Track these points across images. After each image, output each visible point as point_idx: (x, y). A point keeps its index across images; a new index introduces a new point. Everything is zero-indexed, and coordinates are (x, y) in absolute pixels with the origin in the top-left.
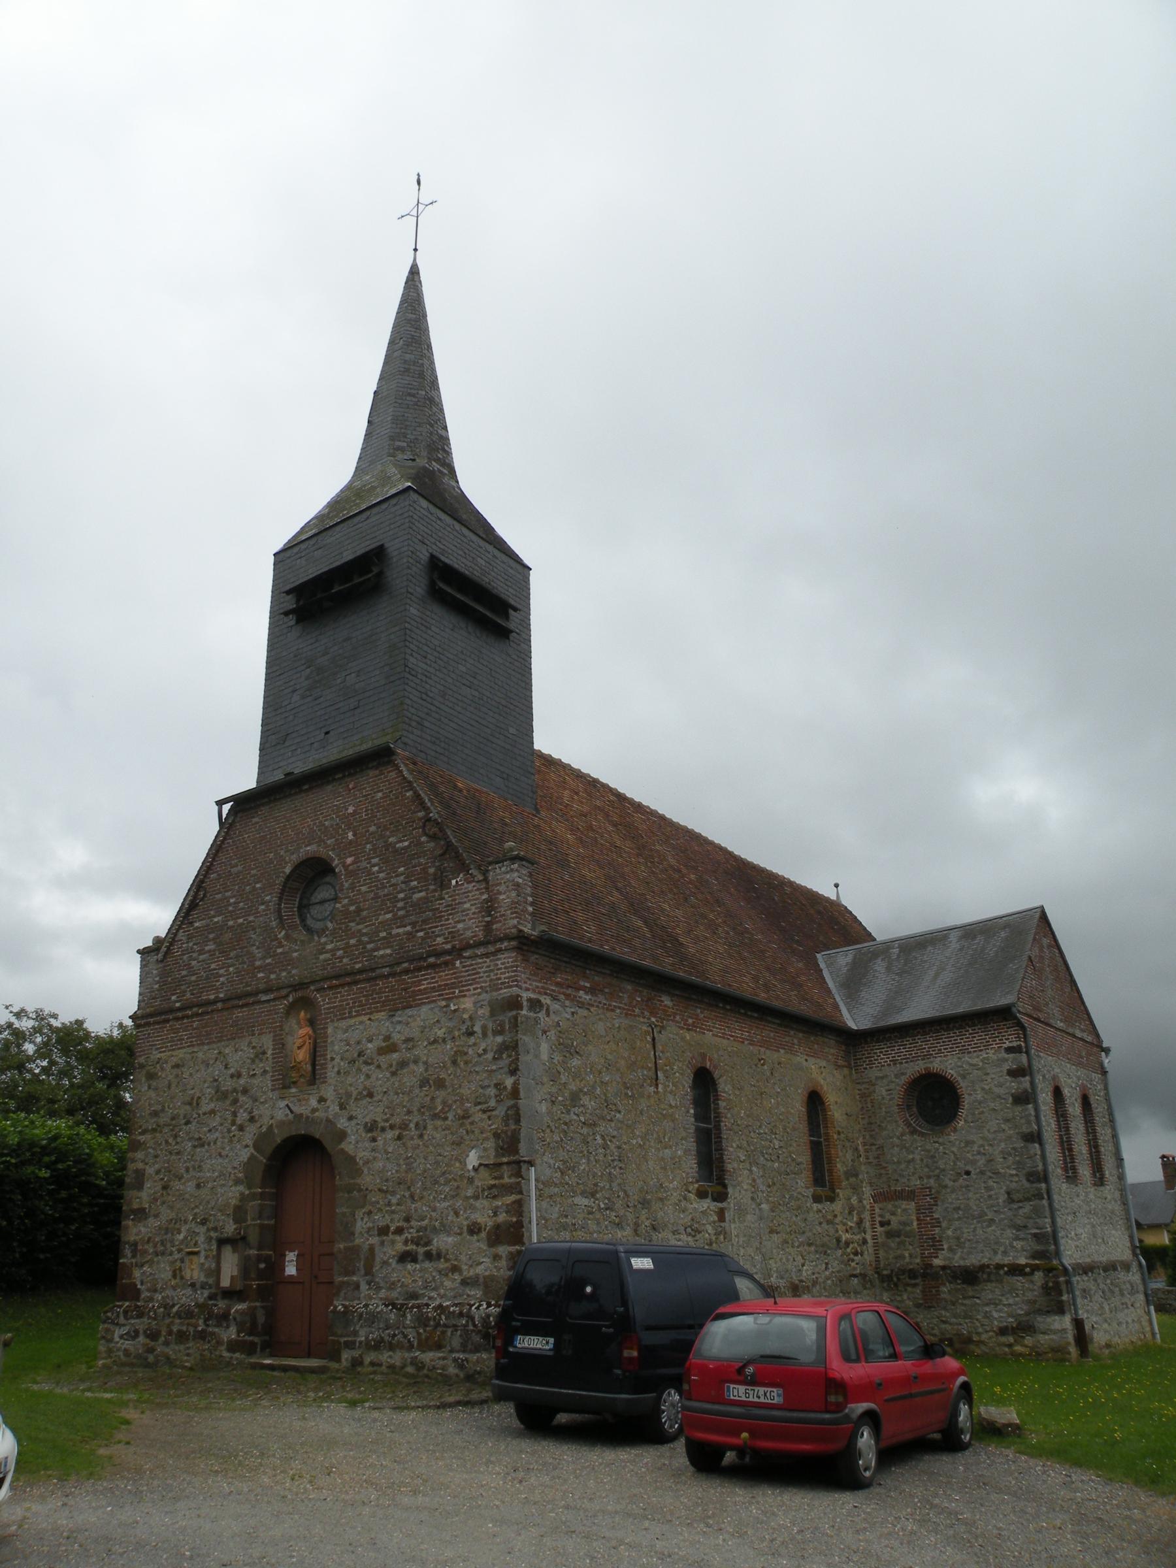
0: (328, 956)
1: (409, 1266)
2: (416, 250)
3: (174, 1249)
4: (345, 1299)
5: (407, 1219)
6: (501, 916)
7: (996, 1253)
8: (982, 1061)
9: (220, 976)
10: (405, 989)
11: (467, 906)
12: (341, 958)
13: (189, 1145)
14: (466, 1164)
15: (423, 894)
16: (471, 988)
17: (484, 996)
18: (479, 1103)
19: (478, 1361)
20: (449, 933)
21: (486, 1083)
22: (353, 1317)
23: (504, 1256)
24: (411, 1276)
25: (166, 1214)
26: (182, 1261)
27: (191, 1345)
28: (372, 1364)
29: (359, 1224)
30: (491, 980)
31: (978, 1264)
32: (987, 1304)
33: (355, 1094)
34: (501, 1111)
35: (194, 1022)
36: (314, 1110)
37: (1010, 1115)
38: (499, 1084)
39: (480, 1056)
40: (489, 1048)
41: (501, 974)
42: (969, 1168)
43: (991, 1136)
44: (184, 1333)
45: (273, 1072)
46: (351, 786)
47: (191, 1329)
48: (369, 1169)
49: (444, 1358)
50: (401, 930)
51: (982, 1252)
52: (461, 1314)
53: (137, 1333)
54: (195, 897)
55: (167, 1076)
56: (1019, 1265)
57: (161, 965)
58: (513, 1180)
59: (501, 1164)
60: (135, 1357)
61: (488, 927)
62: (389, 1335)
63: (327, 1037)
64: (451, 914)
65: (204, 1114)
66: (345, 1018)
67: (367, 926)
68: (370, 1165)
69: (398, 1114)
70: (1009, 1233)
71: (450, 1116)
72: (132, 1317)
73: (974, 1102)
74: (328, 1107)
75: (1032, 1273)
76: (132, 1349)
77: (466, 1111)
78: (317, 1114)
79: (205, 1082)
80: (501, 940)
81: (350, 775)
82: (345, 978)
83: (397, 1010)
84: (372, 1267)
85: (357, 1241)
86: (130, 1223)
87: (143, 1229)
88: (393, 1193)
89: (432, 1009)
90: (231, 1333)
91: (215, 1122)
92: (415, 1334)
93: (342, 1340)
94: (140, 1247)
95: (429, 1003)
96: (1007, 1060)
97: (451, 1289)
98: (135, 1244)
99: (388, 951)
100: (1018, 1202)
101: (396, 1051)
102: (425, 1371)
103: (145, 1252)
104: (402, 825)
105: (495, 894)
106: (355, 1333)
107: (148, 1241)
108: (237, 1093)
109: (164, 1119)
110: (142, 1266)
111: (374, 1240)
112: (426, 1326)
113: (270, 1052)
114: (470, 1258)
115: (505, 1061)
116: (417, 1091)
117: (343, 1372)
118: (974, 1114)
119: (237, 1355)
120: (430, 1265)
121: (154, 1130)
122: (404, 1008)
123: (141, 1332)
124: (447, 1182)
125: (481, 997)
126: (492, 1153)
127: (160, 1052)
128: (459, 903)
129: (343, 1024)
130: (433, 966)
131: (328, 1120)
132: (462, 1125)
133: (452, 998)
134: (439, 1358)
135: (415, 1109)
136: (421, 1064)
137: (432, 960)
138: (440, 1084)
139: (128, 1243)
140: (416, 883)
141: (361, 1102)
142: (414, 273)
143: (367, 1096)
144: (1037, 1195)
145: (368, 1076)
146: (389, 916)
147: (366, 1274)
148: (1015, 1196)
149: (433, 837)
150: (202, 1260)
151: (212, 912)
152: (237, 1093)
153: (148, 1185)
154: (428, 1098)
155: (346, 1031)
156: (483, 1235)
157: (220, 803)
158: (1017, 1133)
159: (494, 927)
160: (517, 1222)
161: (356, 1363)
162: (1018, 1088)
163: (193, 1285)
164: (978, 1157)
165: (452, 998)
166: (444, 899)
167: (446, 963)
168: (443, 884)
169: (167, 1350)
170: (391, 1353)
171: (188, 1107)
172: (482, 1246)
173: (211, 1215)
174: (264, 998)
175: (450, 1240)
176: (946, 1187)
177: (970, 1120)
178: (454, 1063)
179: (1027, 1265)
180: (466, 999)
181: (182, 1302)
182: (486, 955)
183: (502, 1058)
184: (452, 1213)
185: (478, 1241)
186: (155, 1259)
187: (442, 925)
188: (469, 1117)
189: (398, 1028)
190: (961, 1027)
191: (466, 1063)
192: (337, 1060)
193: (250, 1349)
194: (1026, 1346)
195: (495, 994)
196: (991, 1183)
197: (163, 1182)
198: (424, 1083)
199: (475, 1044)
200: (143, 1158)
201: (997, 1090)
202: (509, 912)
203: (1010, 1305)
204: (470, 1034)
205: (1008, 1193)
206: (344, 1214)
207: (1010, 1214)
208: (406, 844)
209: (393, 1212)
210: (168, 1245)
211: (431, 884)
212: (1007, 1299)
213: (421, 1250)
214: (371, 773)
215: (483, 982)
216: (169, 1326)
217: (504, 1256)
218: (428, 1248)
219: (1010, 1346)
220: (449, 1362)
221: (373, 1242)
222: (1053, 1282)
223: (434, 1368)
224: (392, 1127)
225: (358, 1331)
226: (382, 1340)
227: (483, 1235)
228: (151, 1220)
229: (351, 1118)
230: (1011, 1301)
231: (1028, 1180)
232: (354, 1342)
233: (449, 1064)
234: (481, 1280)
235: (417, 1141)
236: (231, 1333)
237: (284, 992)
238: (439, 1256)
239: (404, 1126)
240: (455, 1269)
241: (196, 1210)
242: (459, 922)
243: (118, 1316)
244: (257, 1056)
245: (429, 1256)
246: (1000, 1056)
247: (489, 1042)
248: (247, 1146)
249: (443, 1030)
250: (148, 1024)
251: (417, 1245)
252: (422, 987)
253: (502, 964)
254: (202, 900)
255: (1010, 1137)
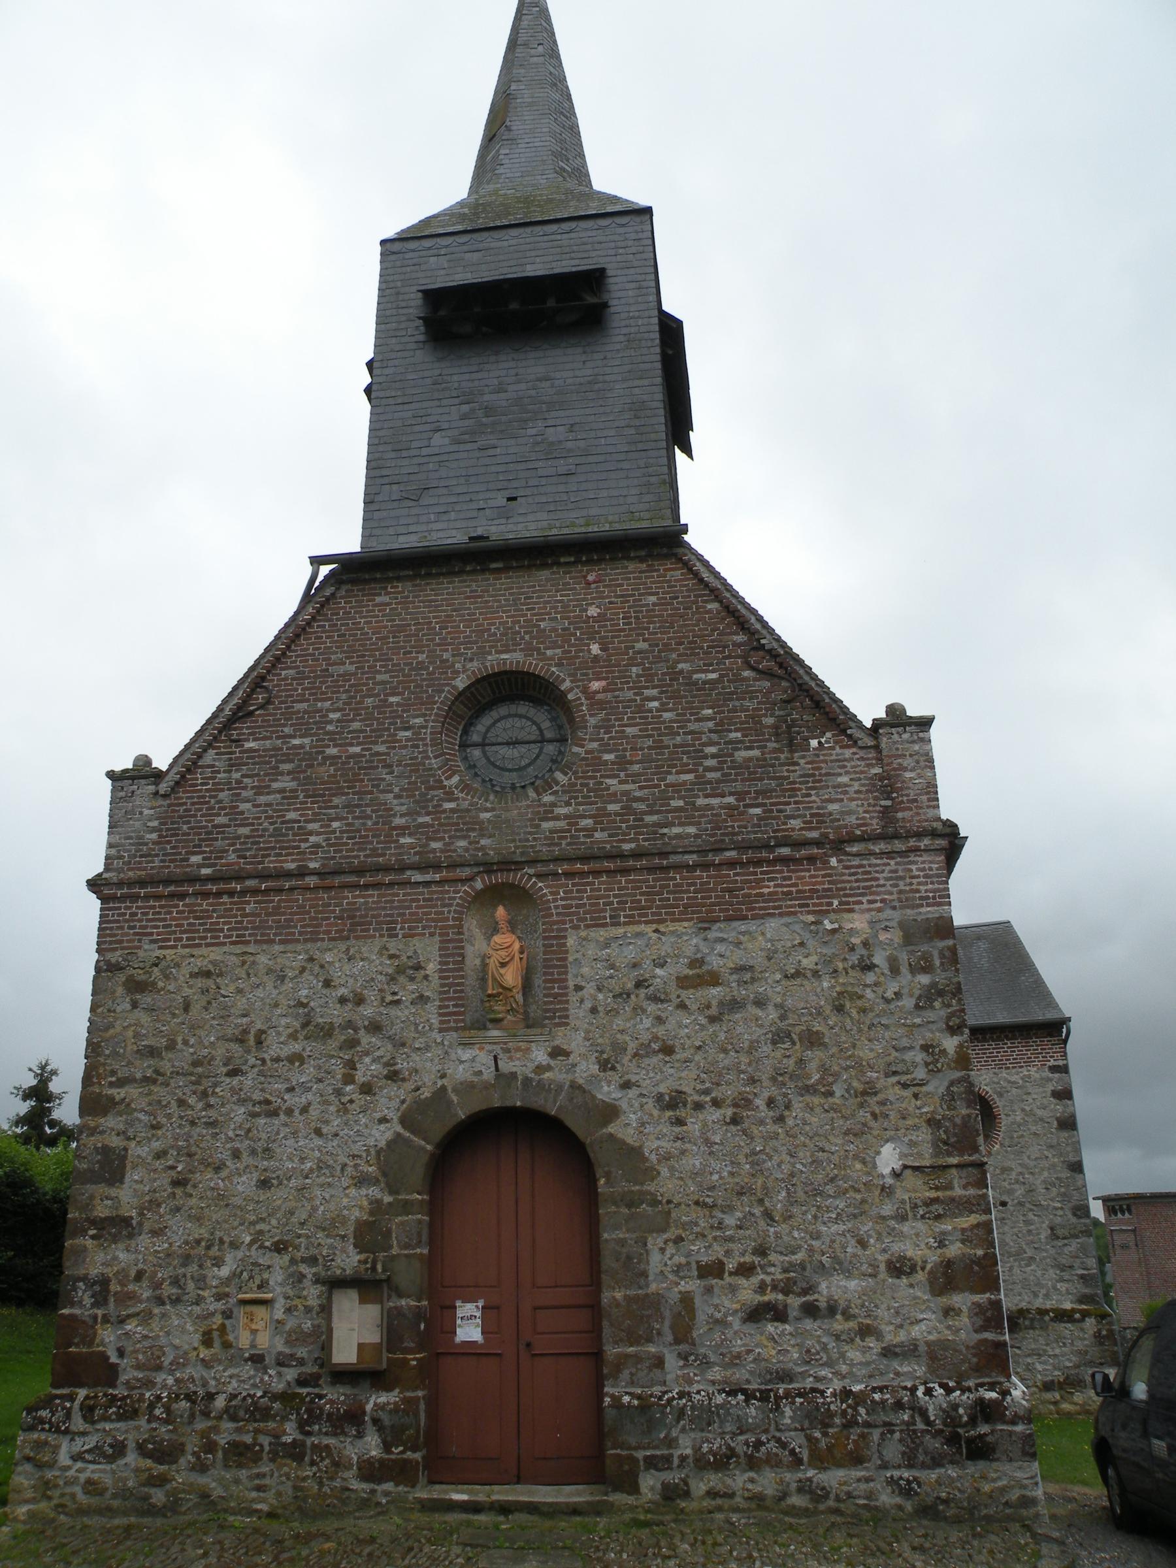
1: (770, 1328)
3: (206, 1294)
4: (632, 1383)
5: (762, 1251)
7: (1036, 1295)
8: (1022, 1079)
9: (311, 833)
10: (730, 891)
11: (844, 779)
12: (590, 832)
14: (875, 1166)
16: (864, 900)
17: (889, 913)
18: (895, 1073)
19: (938, 1482)
20: (812, 815)
21: (905, 1042)
22: (663, 1413)
23: (965, 1309)
25: (180, 1231)
26: (227, 1314)
27: (265, 1469)
28: (712, 1494)
30: (900, 892)
32: (1029, 1355)
33: (632, 1046)
34: (937, 1086)
35: (248, 903)
36: (540, 1069)
37: (1055, 1142)
38: (932, 1046)
39: (888, 1001)
40: (905, 991)
41: (919, 884)
42: (1005, 1198)
43: (1032, 1164)
44: (247, 1447)
45: (441, 1000)
47: (265, 1441)
48: (672, 1169)
49: (868, 1480)
50: (715, 801)
52: (899, 1405)
53: (119, 1449)
54: (245, 701)
55: (179, 989)
56: (1065, 1310)
57: (160, 802)
58: (972, 1191)
60: (115, 1496)
61: (886, 814)
62: (747, 1443)
63: (567, 952)
65: (277, 1060)
66: (604, 925)
68: (672, 1162)
70: (1052, 1273)
71: (838, 1090)
72: (105, 1418)
73: (1013, 1123)
74: (574, 1065)
75: (1082, 1320)
76: (108, 1481)
78: (547, 1075)
79: (276, 1005)
81: (589, 562)
83: (716, 920)
84: (690, 1328)
85: (653, 1287)
86: (89, 1243)
87: (122, 1256)
88: (728, 1209)
90: (372, 1445)
91: (307, 1074)
92: (803, 1441)
93: (640, 1455)
94: (114, 1287)
95: (781, 915)
96: (1051, 1080)
97: (861, 1363)
98: (104, 1282)
99: (692, 830)
100: (1064, 1238)
102: (831, 1503)
103: (132, 1297)
104: (702, 648)
105: (895, 769)
106: (671, 1443)
107: (139, 1276)
108: (356, 1030)
109: (182, 1059)
110: (122, 1321)
111: (692, 1285)
112: (827, 1426)
113: (431, 968)
114: (897, 1313)
115: (938, 1012)
116: (766, 1049)
117: (648, 1511)
118: (1012, 1138)
119: (389, 1486)
120: (816, 1325)
121: (146, 1080)
122: (729, 919)
123: (131, 1445)
127: (161, 948)
129: (602, 934)
130: (785, 860)
131: (574, 1086)
133: (828, 912)
134: (859, 1480)
136: (771, 1008)
137: (785, 851)
138: (813, 1040)
139: (84, 1279)
141: (647, 1061)
143: (659, 1051)
144: (1085, 1231)
145: (659, 1020)
146: (690, 777)
147: (677, 1341)
148: (1060, 1232)
150: (279, 1314)
151: (287, 730)
152: (356, 1030)
153: (133, 1176)
154: (792, 1061)
155: (607, 945)
156: (921, 1276)
157: (317, 561)
158: (1064, 1162)
159: (900, 815)
160: (986, 1255)
161: (672, 1494)
162: (1064, 1112)
163: (257, 1359)
164: (1016, 1186)
165: (828, 912)
166: (797, 764)
167: (811, 859)
169: (202, 1480)
170: (752, 1474)
171: (235, 1047)
172: (919, 1294)
173: (299, 1236)
174: (417, 877)
175: (853, 1284)
177: (1007, 1144)
178: (840, 1009)
179: (1073, 1310)
180: (856, 916)
181: (230, 1389)
182: (890, 855)
183: (932, 1007)
184: (853, 1242)
185: (911, 1286)
186: (156, 1311)
187: (796, 803)
188: (875, 1094)
189: (720, 948)
190: (999, 1039)
192: (590, 989)
193: (401, 1472)
194: (1076, 1404)
195: (909, 912)
196: (1031, 1216)
197: (173, 1173)
198: (779, 1037)
199: (876, 984)
200: (122, 1127)
201: (1040, 1113)
203: (1055, 1355)
204: (869, 967)
205: (1052, 1229)
206: (622, 1242)
207: (1052, 1251)
208: (714, 676)
209: (731, 1239)
210: (191, 1285)
211: (769, 740)
212: (1053, 1349)
213: (794, 1302)
215: (885, 893)
216: (204, 1434)
217: (965, 1309)
218: (809, 1298)
219: (1055, 1403)
221: (689, 1288)
222: (1108, 1330)
223: (849, 1495)
224: (716, 1103)
225: (676, 1439)
226: (732, 1453)
227: (921, 1276)
228: (144, 1241)
229: (626, 1085)
230: (1057, 1351)
231: (1075, 1215)
232: (668, 1459)
233: (828, 1010)
234: (923, 1348)
235: (771, 1127)
236: (372, 1445)
237: (466, 872)
238: (832, 1310)
240: (865, 1331)
241: (261, 1226)
242: (830, 801)
243: (68, 1415)
244: (400, 970)
245: (811, 1310)
246: (1044, 1075)
247: (904, 982)
248: (383, 1120)
250: (135, 898)
251: (786, 1293)
252: (766, 891)
254: (261, 707)
255: (1054, 1166)
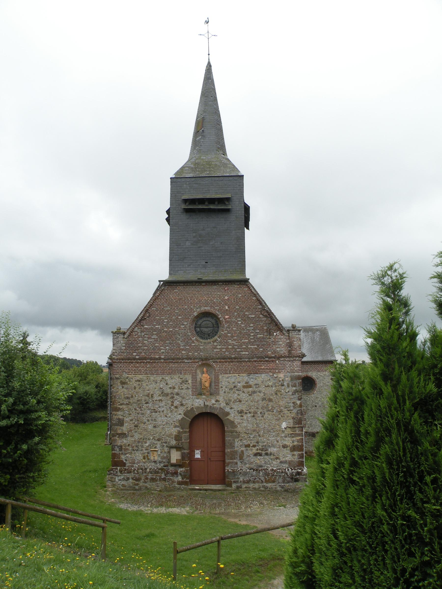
0: (218, 350)
2: (209, 54)
4: (231, 467)
5: (258, 442)
6: (295, 349)
9: (161, 349)
11: (281, 343)
12: (225, 352)
13: (148, 412)
14: (281, 426)
15: (262, 336)
16: (283, 370)
18: (287, 408)
19: (288, 486)
20: (273, 351)
21: (289, 402)
22: (237, 473)
24: (259, 460)
25: (137, 436)
28: (246, 487)
29: (236, 443)
30: (291, 369)
31: (316, 431)
33: (233, 400)
34: (295, 411)
35: (148, 365)
36: (213, 404)
39: (286, 393)
42: (316, 405)
46: (226, 289)
48: (240, 426)
51: (318, 428)
52: (282, 472)
58: (300, 432)
59: (295, 427)
62: (253, 479)
64: (274, 345)
66: (227, 374)
67: (236, 342)
69: (252, 409)
76: (126, 484)
77: (282, 410)
79: (155, 388)
80: (296, 357)
82: (229, 359)
83: (252, 373)
85: (236, 449)
88: (251, 434)
89: (266, 375)
90: (180, 478)
91: (162, 404)
92: (264, 478)
95: (265, 373)
99: (247, 353)
101: (251, 388)
102: (268, 489)
106: (238, 478)
110: (126, 454)
122: (254, 373)
124: (274, 432)
125: (287, 374)
126: (292, 424)
128: (277, 341)
129: (227, 375)
130: (267, 361)
131: (220, 408)
132: (279, 414)
133: (275, 373)
135: (260, 408)
136: (262, 393)
137: (267, 359)
138: (270, 400)
140: (258, 331)
141: (236, 403)
142: (209, 68)
145: (239, 395)
146: (247, 341)
147: (240, 459)
149: (265, 316)
153: (126, 425)
155: (228, 378)
156: (289, 448)
159: (292, 352)
165: (275, 373)
166: (271, 339)
167: (273, 361)
168: (270, 334)
169: (146, 485)
171: (146, 397)
173: (163, 438)
174: (186, 361)
175: (275, 449)
176: (309, 409)
178: (276, 394)
180: (281, 374)
183: (295, 394)
185: (287, 450)
186: (133, 452)
189: (252, 380)
191: (281, 394)
192: (224, 387)
193: (186, 483)
195: (292, 374)
197: (134, 424)
198: (263, 399)
202: (298, 348)
206: (230, 440)
208: (253, 316)
209: (252, 440)
211: (265, 333)
213: (263, 452)
214: (236, 286)
220: (277, 486)
221: (243, 449)
224: (250, 413)
226: (250, 480)
227: (289, 448)
228: (129, 438)
229: (231, 408)
234: (288, 462)
235: (261, 418)
236: (180, 478)
238: (271, 454)
239: (255, 413)
240: (277, 458)
242: (277, 348)
245: (267, 454)
248: (180, 414)
249: (272, 383)
251: (262, 451)
252: (262, 367)
253: (295, 364)
